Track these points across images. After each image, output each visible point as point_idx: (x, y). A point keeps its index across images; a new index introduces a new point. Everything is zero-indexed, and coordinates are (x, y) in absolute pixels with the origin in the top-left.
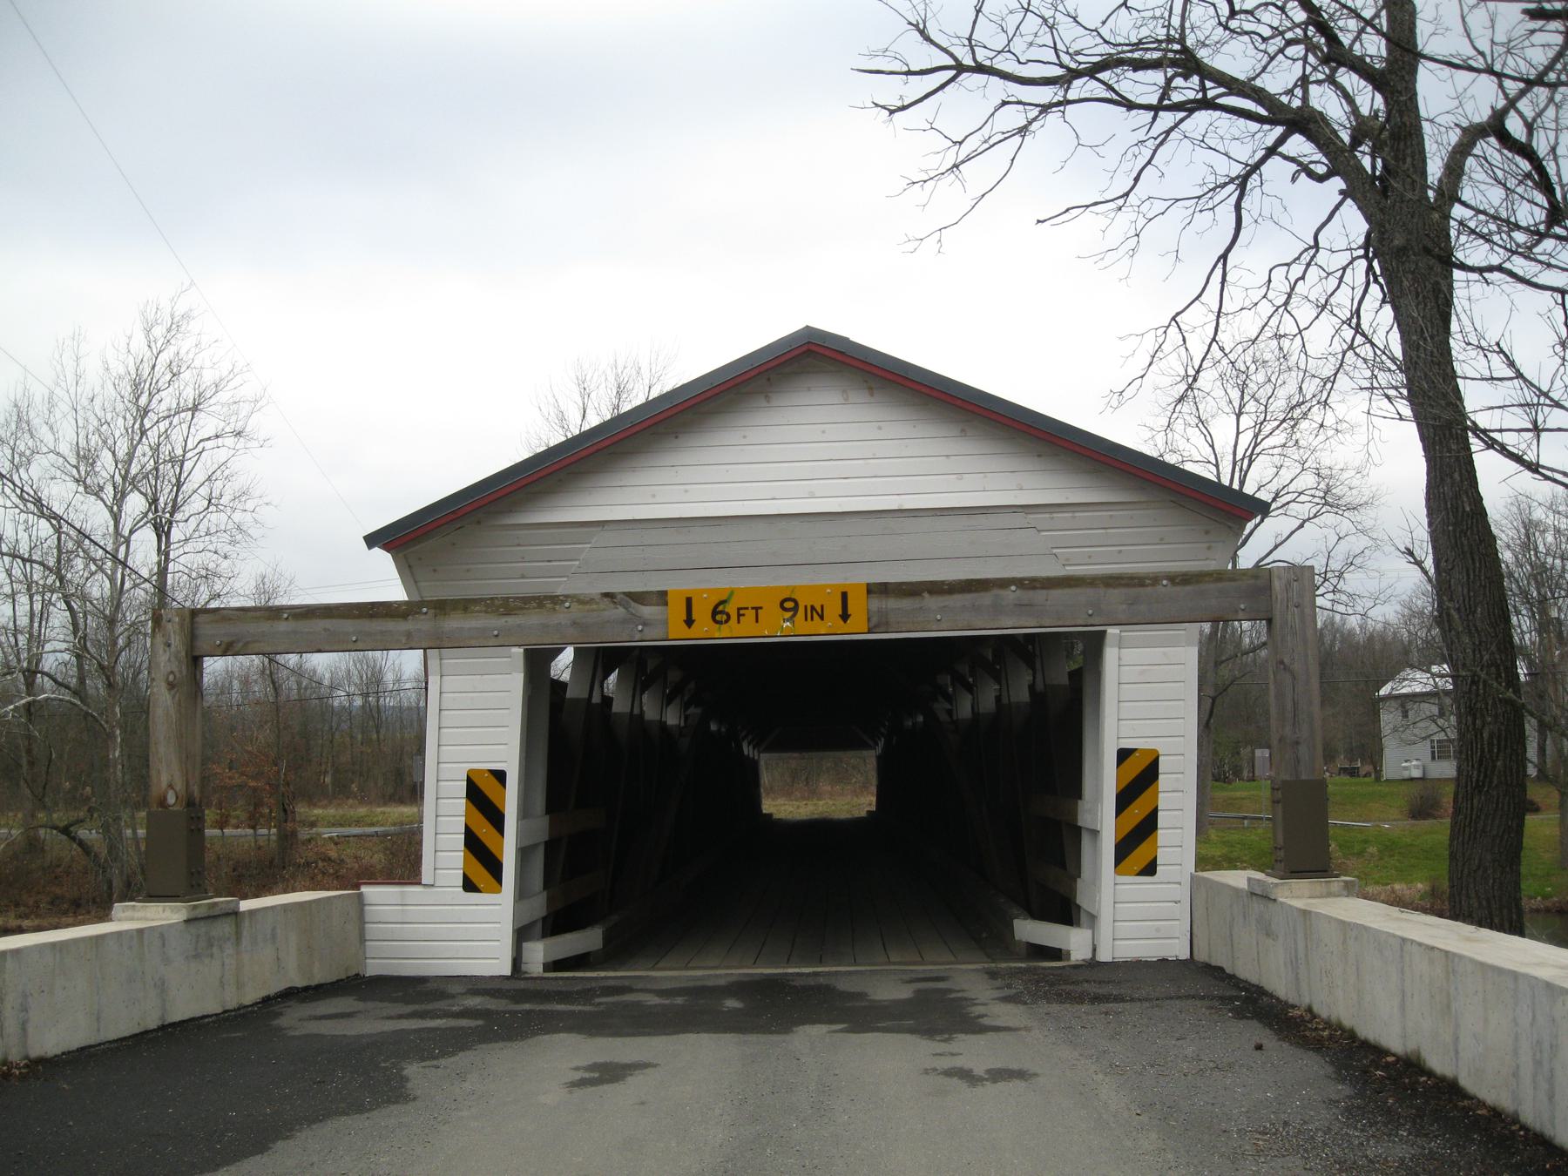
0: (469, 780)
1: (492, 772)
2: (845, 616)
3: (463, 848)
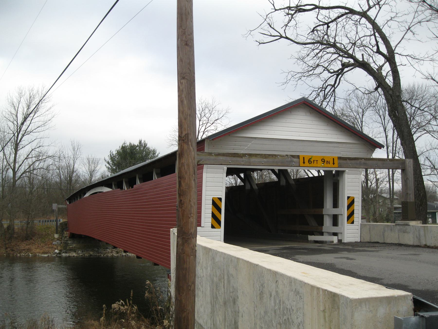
0: (213, 200)
1: (218, 198)
2: (334, 164)
3: (211, 217)
